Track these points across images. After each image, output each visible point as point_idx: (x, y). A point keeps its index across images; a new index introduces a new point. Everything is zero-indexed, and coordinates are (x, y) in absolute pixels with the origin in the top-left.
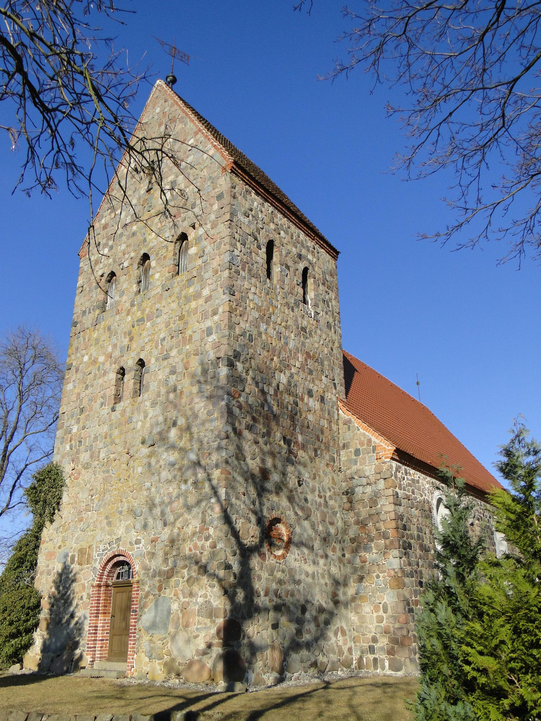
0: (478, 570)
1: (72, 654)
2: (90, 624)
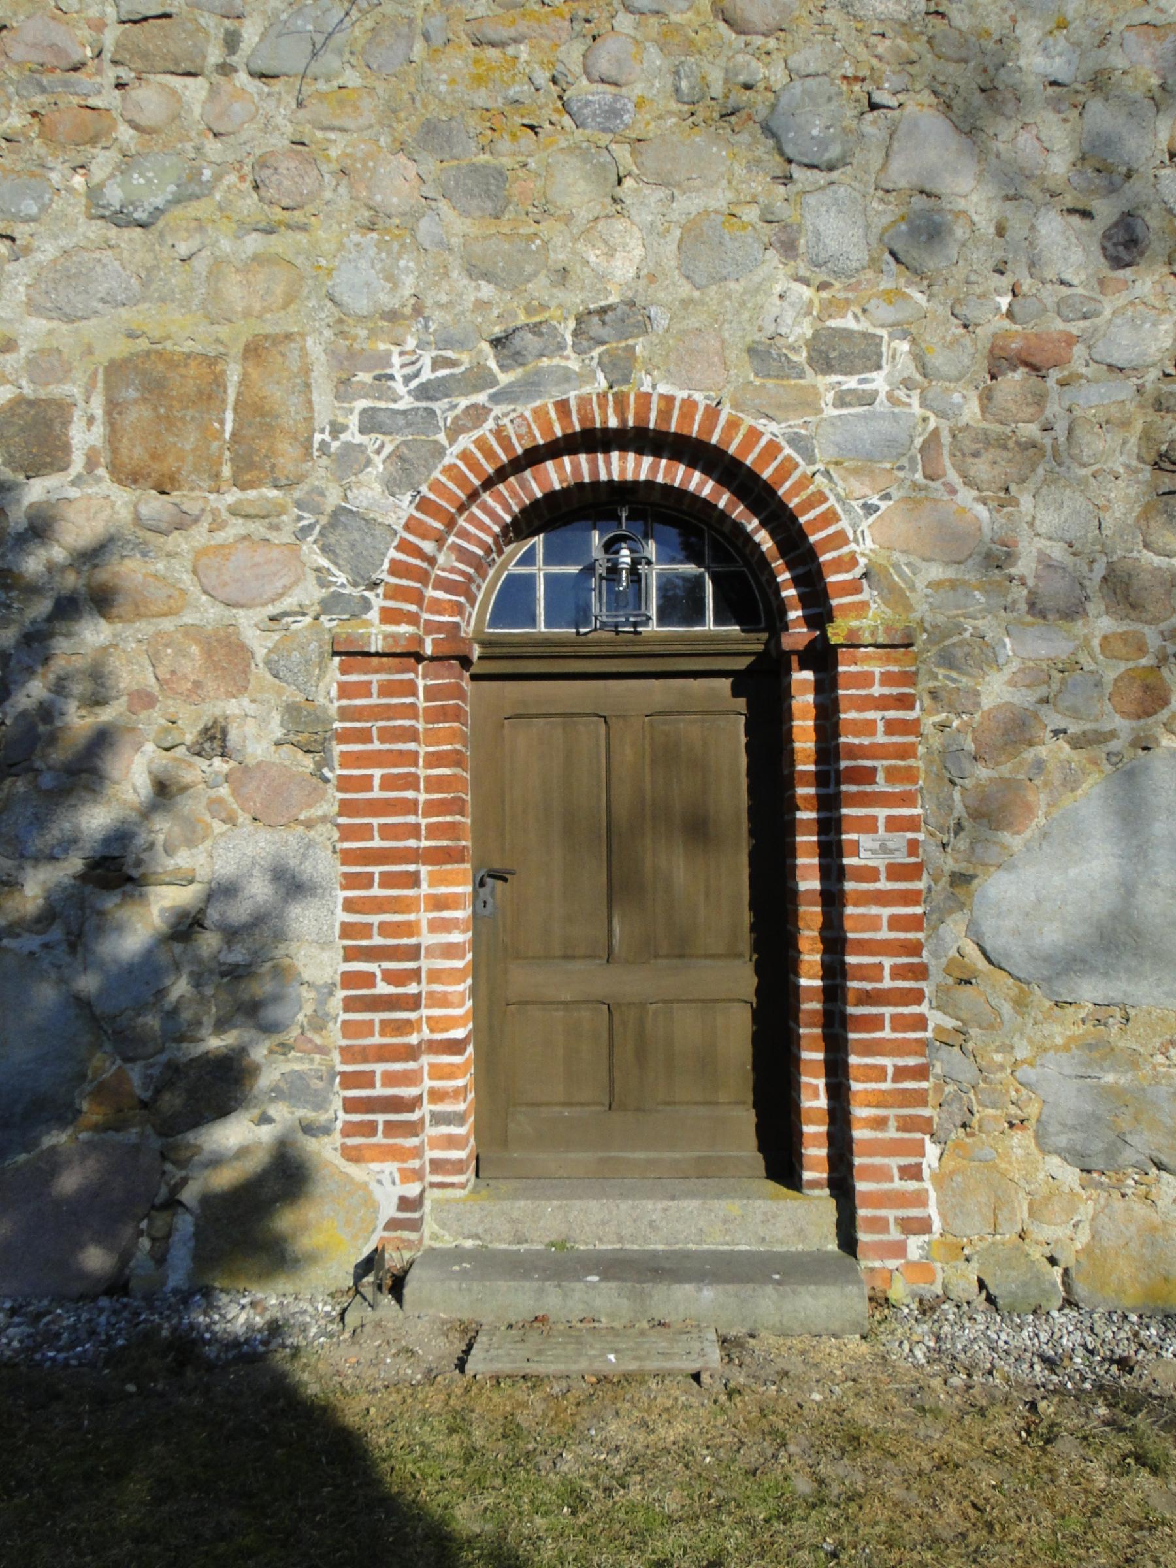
0: (130, 632)
1: (145, 1178)
2: (348, 930)
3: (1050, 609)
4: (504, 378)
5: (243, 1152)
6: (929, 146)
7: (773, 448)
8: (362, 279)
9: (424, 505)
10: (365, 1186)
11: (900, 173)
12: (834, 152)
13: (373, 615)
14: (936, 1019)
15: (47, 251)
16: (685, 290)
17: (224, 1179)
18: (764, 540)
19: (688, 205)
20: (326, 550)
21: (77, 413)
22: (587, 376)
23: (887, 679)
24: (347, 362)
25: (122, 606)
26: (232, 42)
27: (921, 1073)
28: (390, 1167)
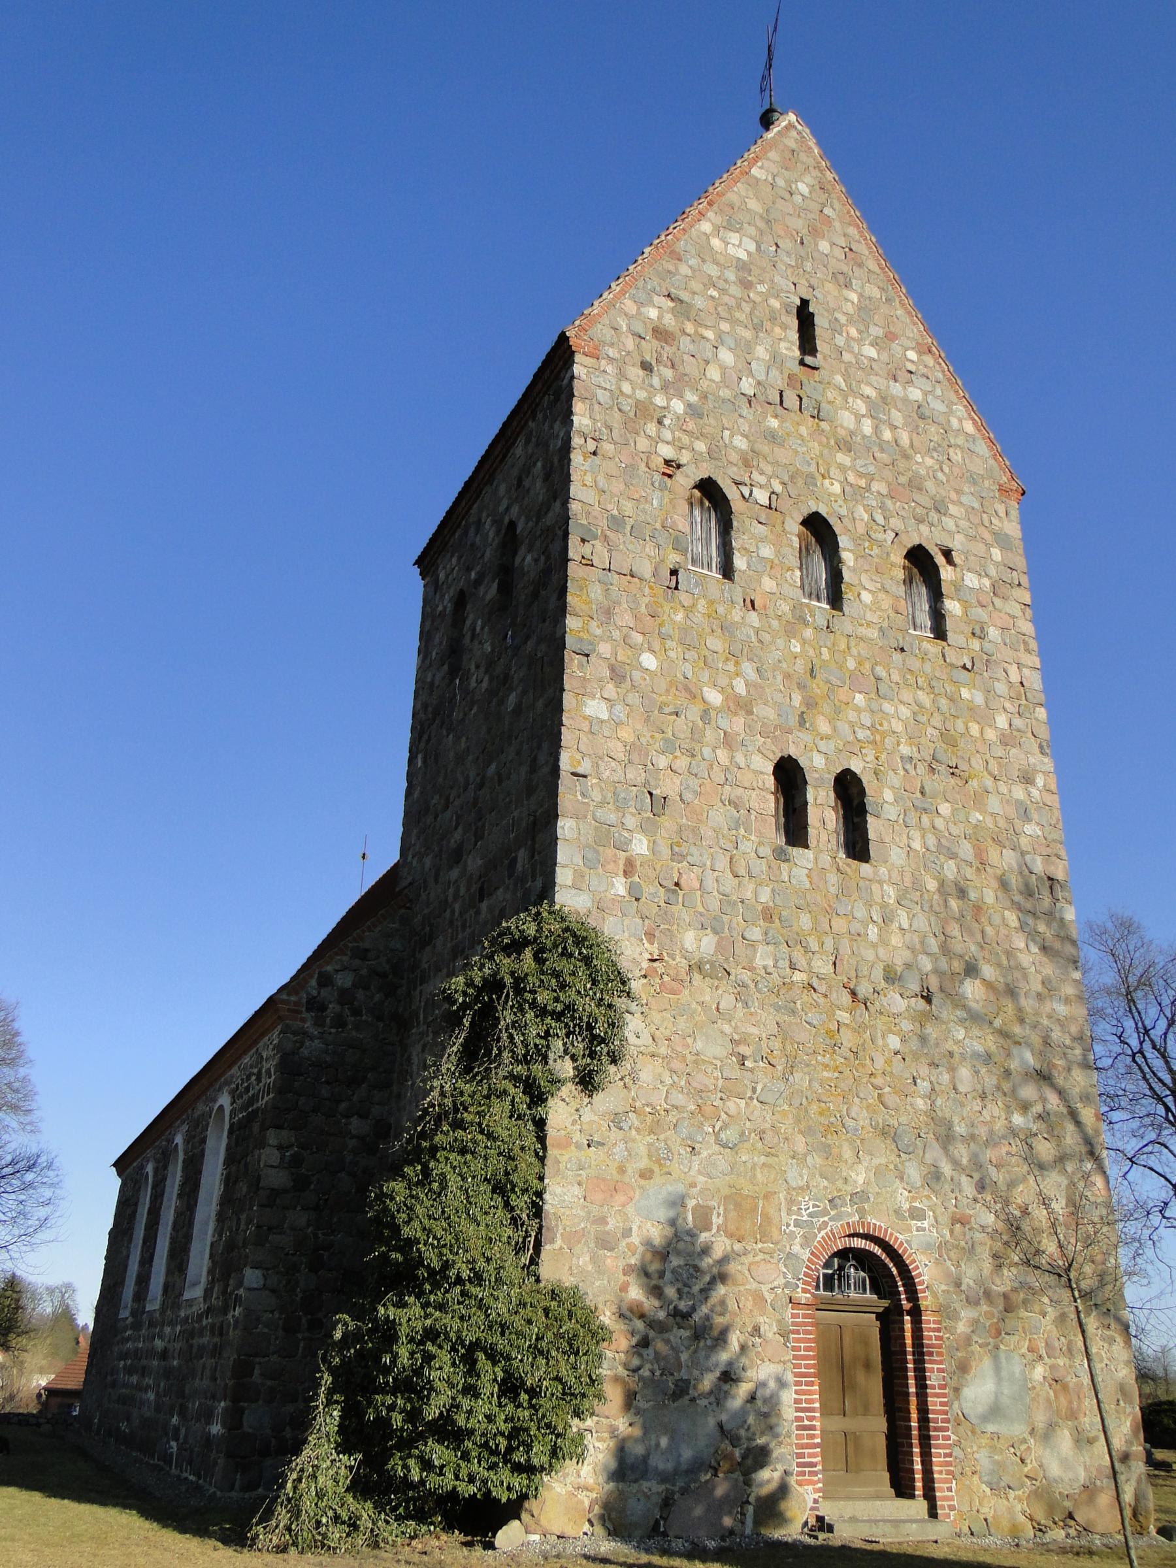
3: (972, 1302)
4: (833, 1213)
5: (768, 1481)
6: (934, 1153)
7: (901, 1244)
8: (796, 1177)
9: (813, 1253)
10: (802, 1495)
11: (929, 1158)
12: (911, 1149)
13: (799, 1290)
14: (953, 1437)
15: (705, 1154)
16: (877, 1189)
17: (765, 1491)
18: (894, 1271)
19: (876, 1161)
20: (786, 1266)
21: (715, 1212)
22: (852, 1215)
23: (935, 1322)
24: (791, 1202)
25: (730, 1282)
26: (754, 1090)
27: (950, 1455)
28: (810, 1488)
